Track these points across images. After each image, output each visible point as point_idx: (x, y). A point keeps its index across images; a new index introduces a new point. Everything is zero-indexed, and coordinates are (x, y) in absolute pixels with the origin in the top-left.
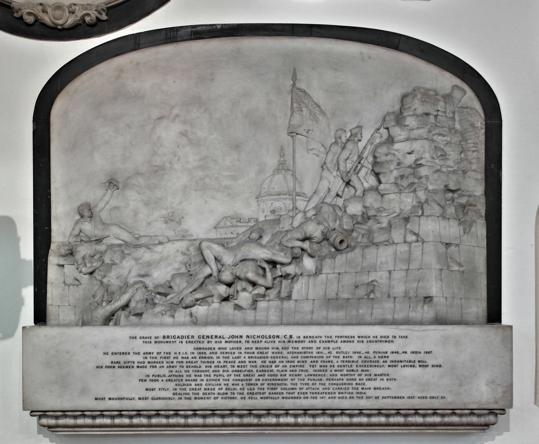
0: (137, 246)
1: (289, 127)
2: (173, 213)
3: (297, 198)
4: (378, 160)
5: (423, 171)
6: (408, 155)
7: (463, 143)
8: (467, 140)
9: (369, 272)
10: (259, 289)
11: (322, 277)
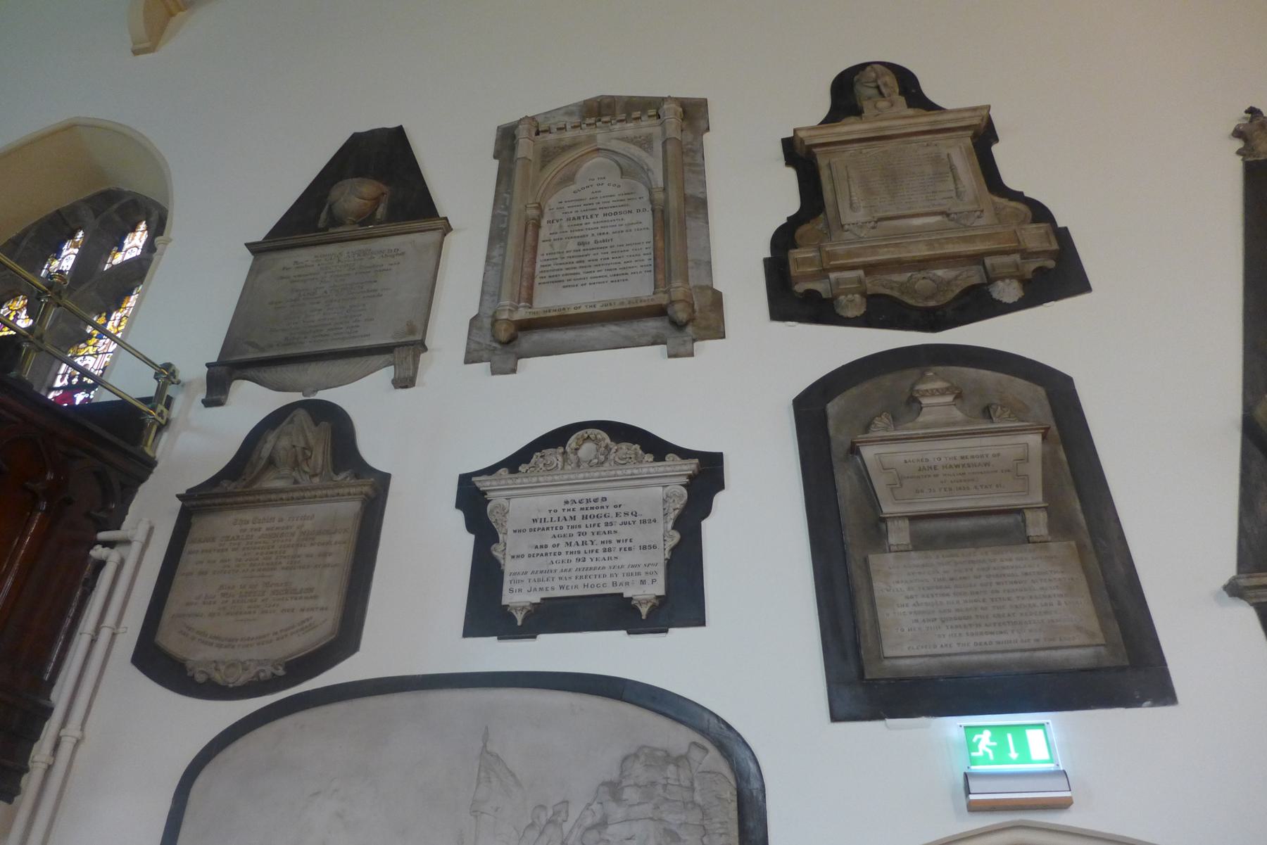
1: (472, 805)
6: (628, 842)
7: (706, 822)
8: (711, 819)
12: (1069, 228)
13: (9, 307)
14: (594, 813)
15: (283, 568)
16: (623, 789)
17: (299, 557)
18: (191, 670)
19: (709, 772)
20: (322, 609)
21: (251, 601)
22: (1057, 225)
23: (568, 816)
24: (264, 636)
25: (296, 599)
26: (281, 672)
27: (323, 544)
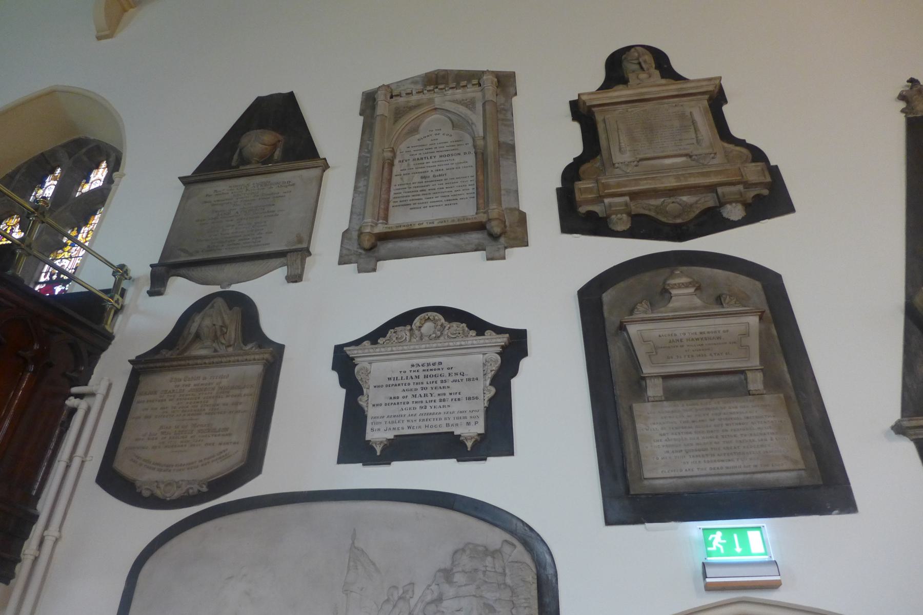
1: (344, 586)
6: (457, 613)
7: (514, 598)
8: (518, 596)
12: (778, 166)
13: (6, 223)
14: (433, 592)
15: (206, 414)
16: (453, 574)
17: (218, 405)
18: (139, 488)
19: (516, 562)
20: (235, 443)
21: (183, 437)
22: (770, 164)
23: (413, 594)
24: (192, 463)
25: (216, 436)
26: (205, 489)
27: (235, 396)
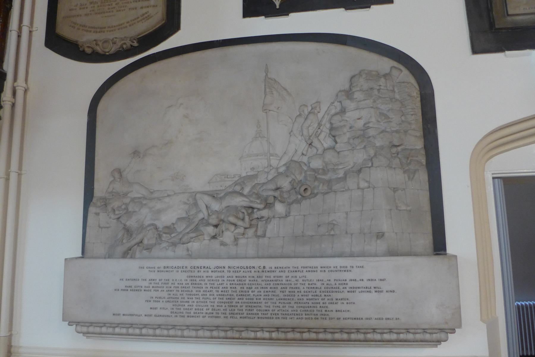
0: (151, 199)
1: (263, 106)
2: (178, 173)
3: (271, 157)
4: (334, 126)
5: (371, 132)
6: (358, 121)
7: (402, 109)
9: (329, 214)
10: (239, 229)
11: (290, 219)
14: (336, 107)
16: (353, 93)
18: (81, 47)
19: (403, 82)
20: (154, 6)
21: (109, 5)
23: (320, 109)
24: (121, 25)
26: (136, 44)
